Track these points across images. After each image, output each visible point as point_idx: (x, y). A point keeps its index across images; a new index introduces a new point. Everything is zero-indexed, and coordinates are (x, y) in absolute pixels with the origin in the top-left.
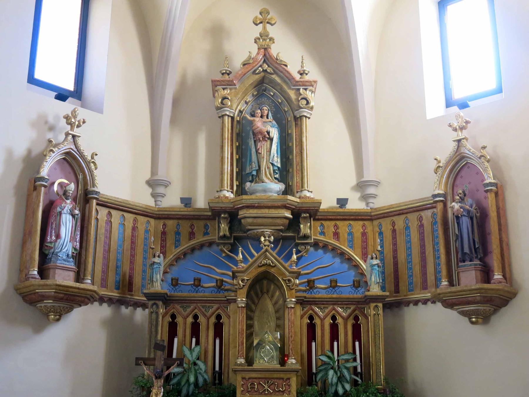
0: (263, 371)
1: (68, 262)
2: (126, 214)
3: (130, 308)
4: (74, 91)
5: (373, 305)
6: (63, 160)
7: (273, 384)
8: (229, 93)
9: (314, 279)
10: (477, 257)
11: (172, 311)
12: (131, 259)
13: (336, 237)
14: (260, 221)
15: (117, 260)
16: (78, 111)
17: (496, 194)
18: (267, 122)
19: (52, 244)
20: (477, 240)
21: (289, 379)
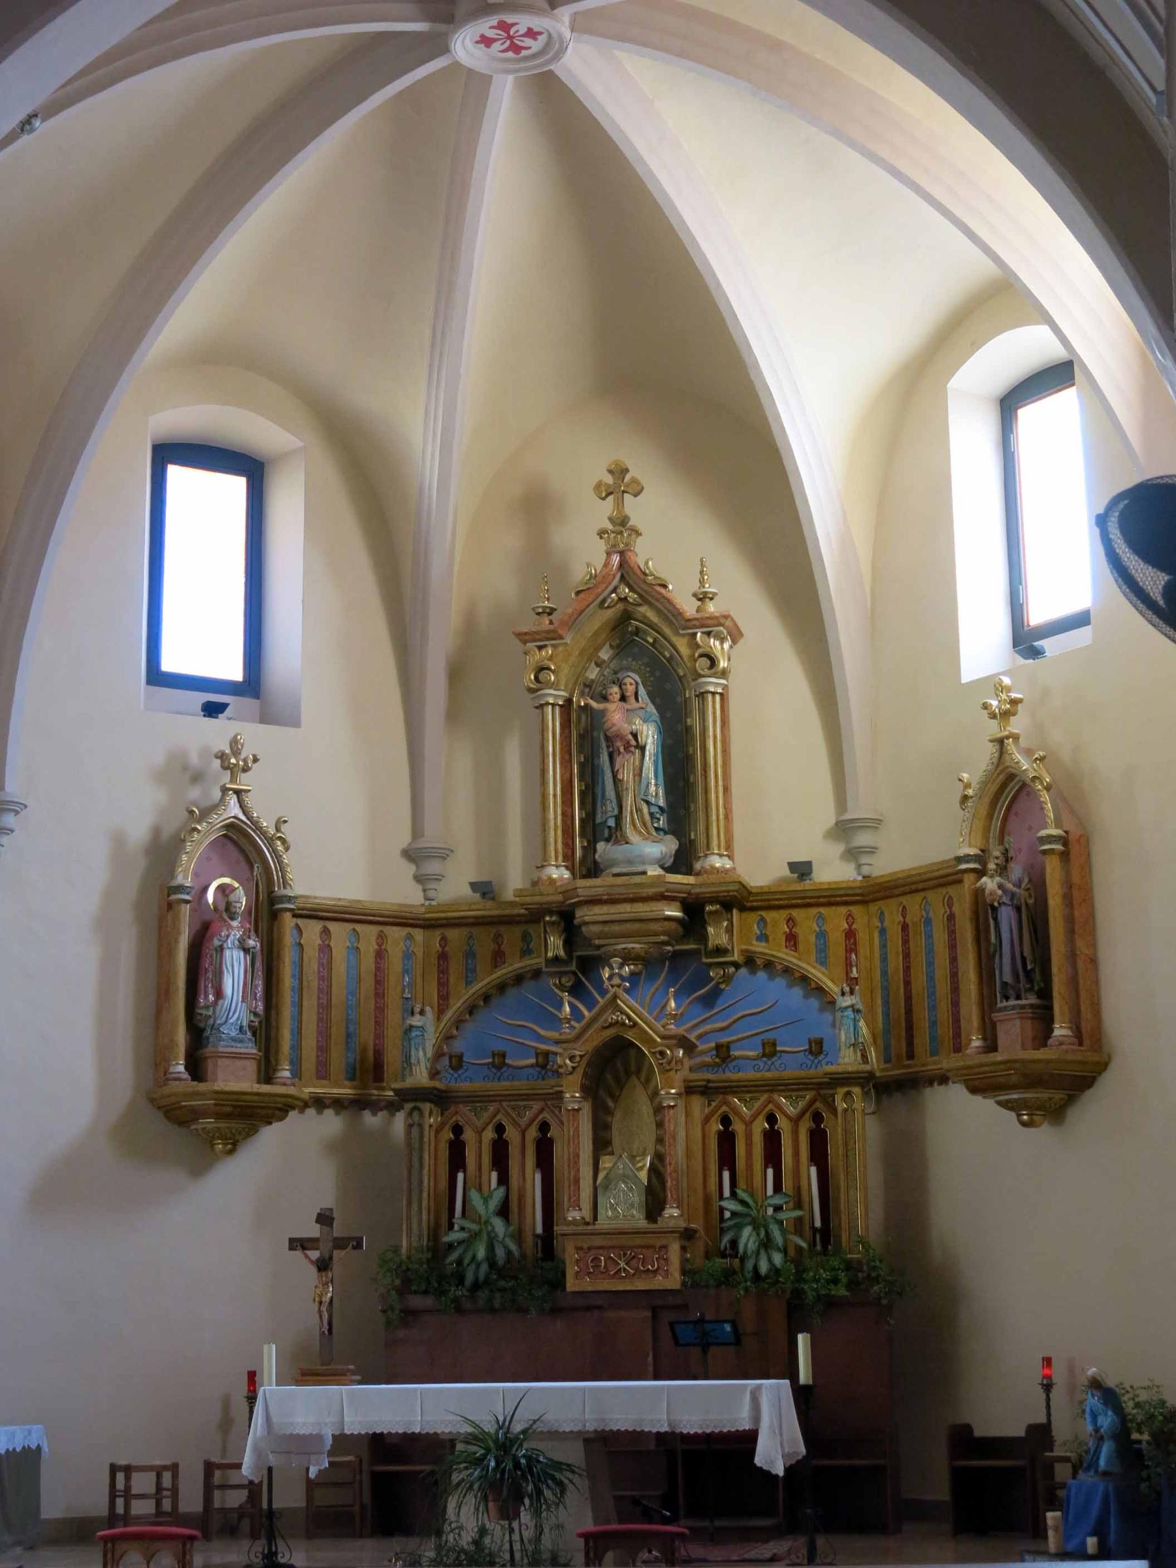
0: (614, 1234)
1: (241, 1041)
2: (358, 927)
3: (380, 1114)
4: (244, 681)
5: (841, 1091)
6: (225, 841)
7: (634, 1257)
8: (552, 654)
9: (729, 1043)
10: (1031, 989)
11: (454, 1119)
12: (376, 1017)
13: (792, 943)
14: (616, 928)
15: (348, 1021)
16: (242, 741)
17: (1065, 856)
18: (636, 709)
19: (208, 1011)
20: (1027, 952)
21: (665, 1247)
